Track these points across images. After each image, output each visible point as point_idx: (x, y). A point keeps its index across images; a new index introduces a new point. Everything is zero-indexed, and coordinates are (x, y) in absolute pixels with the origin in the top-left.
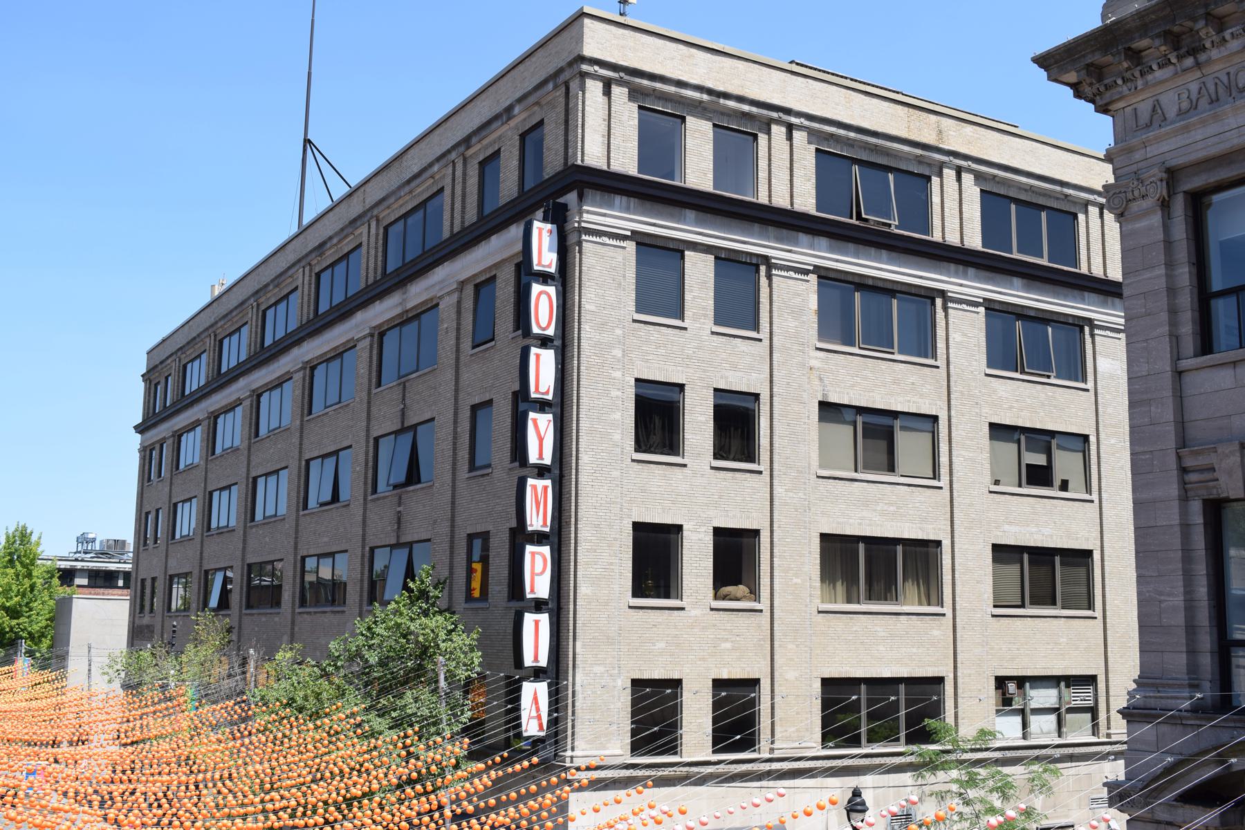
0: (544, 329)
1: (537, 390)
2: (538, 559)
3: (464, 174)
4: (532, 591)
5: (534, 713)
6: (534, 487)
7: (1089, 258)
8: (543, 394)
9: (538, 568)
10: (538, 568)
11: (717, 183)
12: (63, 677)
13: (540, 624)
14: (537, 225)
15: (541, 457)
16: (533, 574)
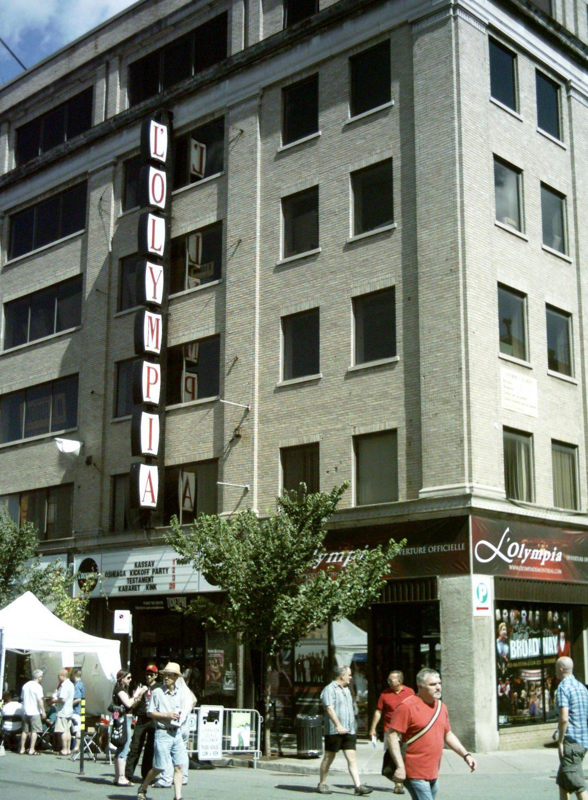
0: (157, 202)
1: (153, 247)
2: (152, 372)
3: (398, 592)
4: (148, 396)
5: (149, 489)
6: (150, 318)
7: (577, 241)
8: (156, 250)
9: (152, 379)
10: (152, 379)
11: (275, 131)
12: (86, 233)
13: (153, 421)
14: (153, 124)
15: (150, 449)
16: (149, 384)
